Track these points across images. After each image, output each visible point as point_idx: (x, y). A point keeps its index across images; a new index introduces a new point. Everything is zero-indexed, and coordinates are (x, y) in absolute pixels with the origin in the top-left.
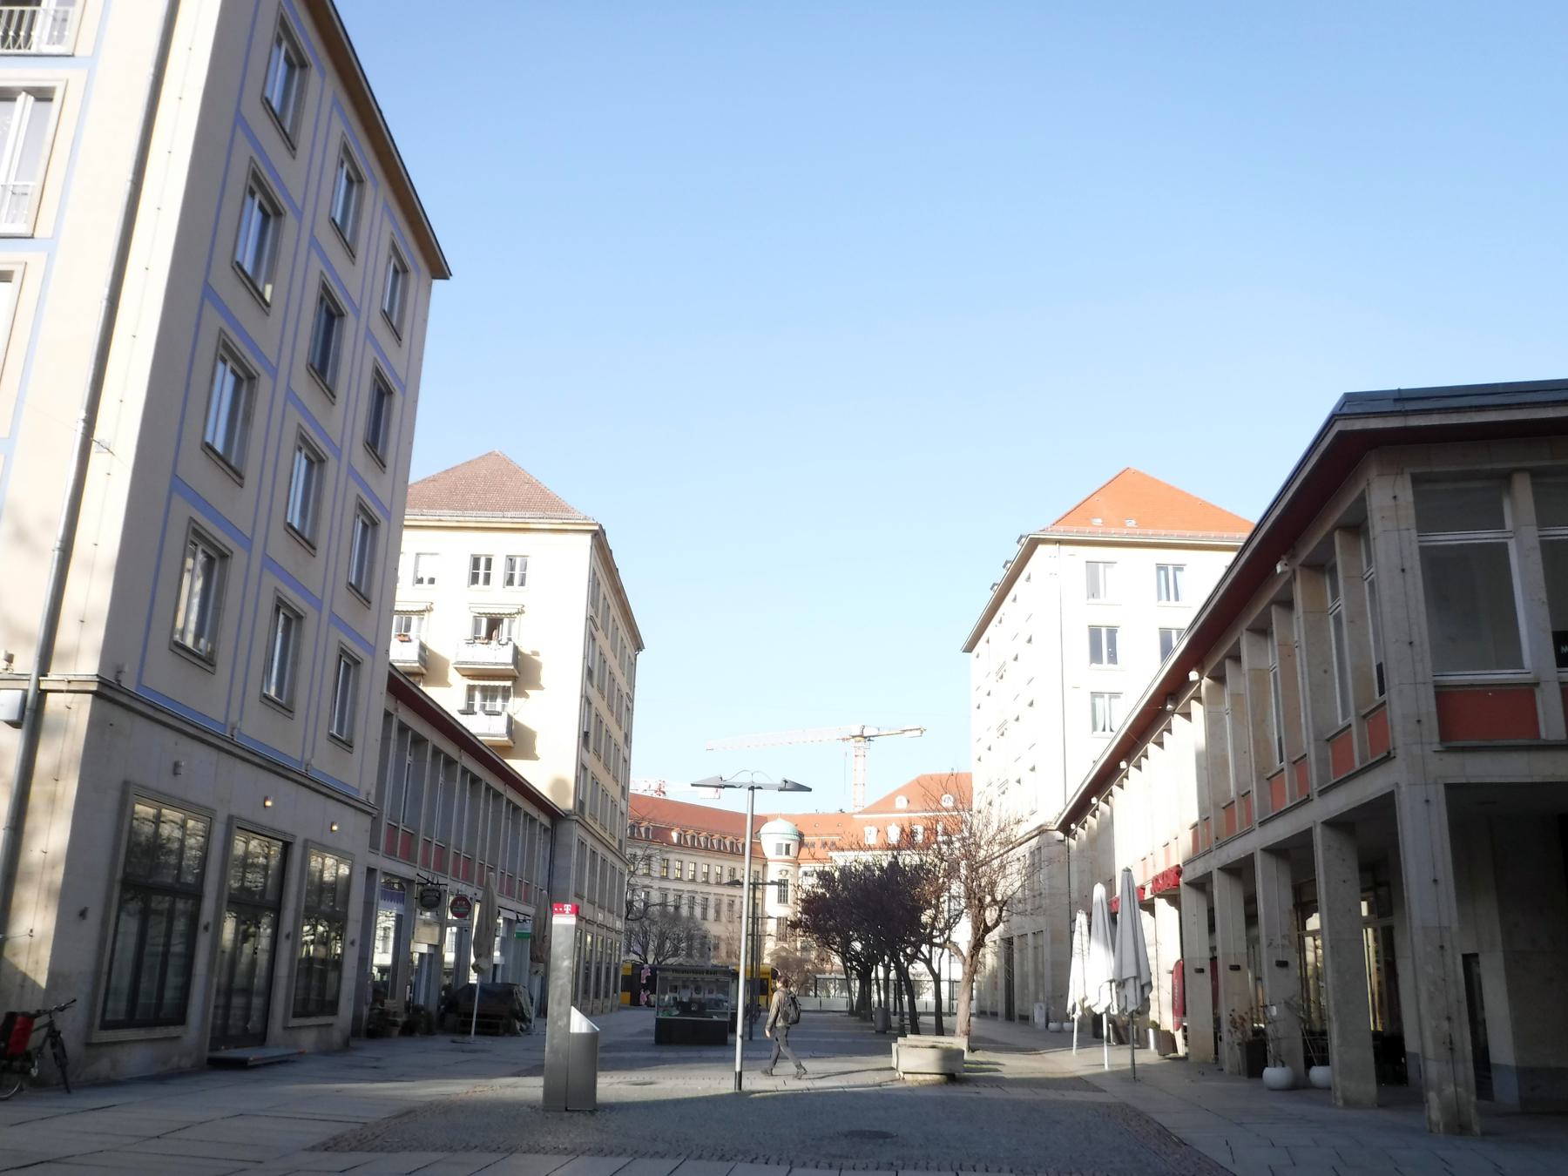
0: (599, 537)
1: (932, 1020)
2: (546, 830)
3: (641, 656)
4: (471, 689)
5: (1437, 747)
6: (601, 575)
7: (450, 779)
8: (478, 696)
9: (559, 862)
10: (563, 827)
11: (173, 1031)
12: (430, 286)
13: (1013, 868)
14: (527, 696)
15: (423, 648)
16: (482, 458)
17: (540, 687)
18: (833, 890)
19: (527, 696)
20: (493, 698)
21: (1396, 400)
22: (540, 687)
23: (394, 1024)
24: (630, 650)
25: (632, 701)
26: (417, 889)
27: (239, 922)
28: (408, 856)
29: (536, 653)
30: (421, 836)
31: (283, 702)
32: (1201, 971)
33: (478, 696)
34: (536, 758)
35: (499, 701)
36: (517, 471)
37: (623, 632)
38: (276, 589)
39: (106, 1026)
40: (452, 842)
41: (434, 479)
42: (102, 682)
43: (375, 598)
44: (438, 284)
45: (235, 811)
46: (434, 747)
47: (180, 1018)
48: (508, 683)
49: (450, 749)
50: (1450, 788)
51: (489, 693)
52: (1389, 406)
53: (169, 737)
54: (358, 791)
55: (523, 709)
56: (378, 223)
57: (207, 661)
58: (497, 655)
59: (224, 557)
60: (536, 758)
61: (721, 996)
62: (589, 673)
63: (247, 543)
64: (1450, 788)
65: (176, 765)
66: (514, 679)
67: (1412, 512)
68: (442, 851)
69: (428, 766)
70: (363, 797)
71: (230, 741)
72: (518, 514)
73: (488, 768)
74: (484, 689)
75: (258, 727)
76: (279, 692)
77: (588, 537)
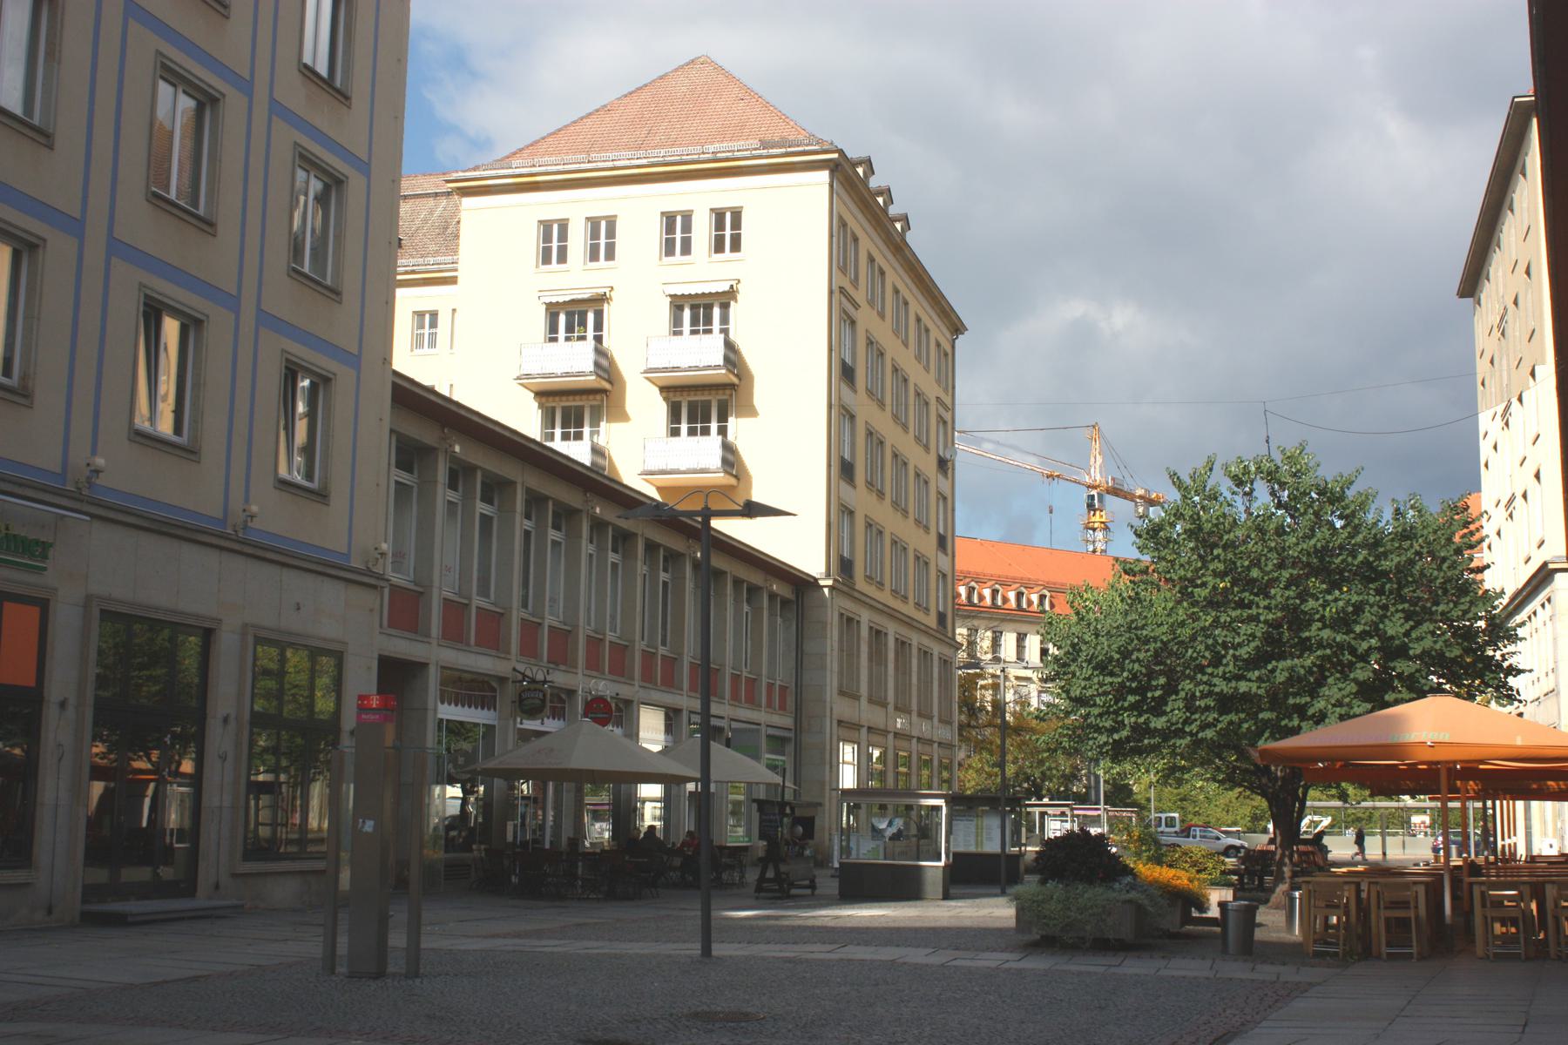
0: (851, 180)
1: (1451, 817)
2: (785, 603)
3: (961, 341)
6: (858, 223)
7: (629, 555)
13: (1172, 872)
18: (1472, 571)
24: (938, 332)
25: (951, 409)
26: (511, 689)
28: (752, 701)
30: (765, 680)
31: (315, 485)
37: (918, 306)
38: (142, 286)
40: (764, 672)
43: (350, 286)
46: (529, 491)
49: (756, 578)
54: (348, 556)
57: (191, 452)
59: (198, 323)
62: (844, 373)
63: (233, 303)
68: (752, 682)
69: (765, 613)
70: (356, 563)
71: (243, 542)
73: (683, 538)
75: (274, 518)
76: (178, 429)
77: (824, 175)
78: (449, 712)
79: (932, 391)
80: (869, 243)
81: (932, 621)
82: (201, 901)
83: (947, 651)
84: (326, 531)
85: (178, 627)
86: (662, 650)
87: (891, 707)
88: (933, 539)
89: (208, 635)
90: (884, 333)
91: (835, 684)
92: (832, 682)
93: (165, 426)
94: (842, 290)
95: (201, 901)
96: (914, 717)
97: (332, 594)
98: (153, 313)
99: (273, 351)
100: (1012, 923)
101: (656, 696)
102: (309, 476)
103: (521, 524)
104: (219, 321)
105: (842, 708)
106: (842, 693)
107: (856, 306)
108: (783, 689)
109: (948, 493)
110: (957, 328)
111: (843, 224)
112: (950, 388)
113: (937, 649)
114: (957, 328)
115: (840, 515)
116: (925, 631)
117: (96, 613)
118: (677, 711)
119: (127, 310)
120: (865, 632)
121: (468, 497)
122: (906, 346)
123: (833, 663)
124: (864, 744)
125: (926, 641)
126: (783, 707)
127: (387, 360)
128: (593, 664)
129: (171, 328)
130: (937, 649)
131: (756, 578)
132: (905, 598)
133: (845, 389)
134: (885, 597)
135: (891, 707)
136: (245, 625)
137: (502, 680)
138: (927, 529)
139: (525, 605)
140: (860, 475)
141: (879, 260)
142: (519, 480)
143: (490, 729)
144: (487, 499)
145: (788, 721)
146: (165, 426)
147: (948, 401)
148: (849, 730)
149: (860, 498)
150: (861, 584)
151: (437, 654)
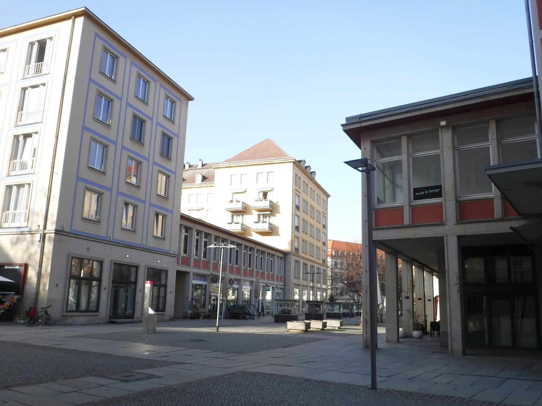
2: (281, 258)
4: (259, 215)
5: (455, 223)
8: (261, 217)
9: (287, 267)
10: (288, 257)
11: (96, 314)
12: (187, 104)
14: (276, 216)
15: (271, 202)
16: (264, 141)
17: (280, 213)
19: (276, 216)
20: (266, 217)
21: (360, 118)
22: (280, 213)
23: (201, 315)
24: (323, 196)
27: (153, 285)
28: (273, 279)
29: (278, 202)
32: (430, 300)
33: (261, 217)
34: (279, 235)
35: (268, 218)
36: (274, 144)
39: (68, 311)
41: (248, 150)
42: (56, 230)
44: (190, 102)
45: (112, 259)
47: (97, 310)
48: (269, 213)
50: (459, 237)
51: (265, 216)
52: (358, 120)
53: (85, 242)
54: (141, 245)
55: (275, 220)
56: (157, 92)
58: (265, 204)
60: (279, 235)
61: (318, 309)
64: (459, 237)
65: (88, 248)
66: (271, 211)
67: (369, 153)
72: (269, 159)
74: (263, 215)
77: (292, 164)
78: (195, 282)
79: (321, 210)
80: (304, 178)
81: (321, 262)
82: (135, 319)
83: (325, 268)
84: (165, 246)
85: (130, 266)
86: (271, 273)
87: (309, 281)
88: (321, 243)
89: (137, 267)
90: (308, 198)
91: (293, 276)
92: (292, 275)
93: (159, 235)
94: (296, 189)
95: (135, 319)
96: (316, 283)
97: (166, 258)
98: (157, 215)
99: (153, 210)
100: (378, 328)
101: (247, 278)
102: (132, 228)
103: (267, 258)
104: (141, 206)
105: (295, 281)
106: (295, 277)
107: (300, 193)
108: (281, 277)
109: (326, 233)
110: (328, 196)
111: (296, 175)
112: (326, 209)
113: (322, 268)
114: (328, 196)
115: (295, 238)
116: (319, 264)
117: (113, 263)
118: (253, 282)
119: (153, 215)
120: (301, 264)
121: (269, 258)
122: (307, 195)
123: (292, 271)
124: (301, 290)
125: (319, 266)
126: (281, 280)
127: (179, 211)
128: (268, 278)
129: (160, 217)
130: (322, 268)
131: (274, 253)
132: (306, 254)
133: (297, 211)
134: (308, 256)
135: (309, 281)
136: (112, 261)
137: (208, 275)
138: (320, 241)
139: (230, 262)
140: (301, 229)
141: (306, 182)
142: (213, 234)
143: (206, 285)
144: (250, 251)
145: (282, 284)
146: (159, 235)
147: (326, 212)
148: (297, 285)
149: (301, 235)
150: (301, 254)
151: (192, 270)
